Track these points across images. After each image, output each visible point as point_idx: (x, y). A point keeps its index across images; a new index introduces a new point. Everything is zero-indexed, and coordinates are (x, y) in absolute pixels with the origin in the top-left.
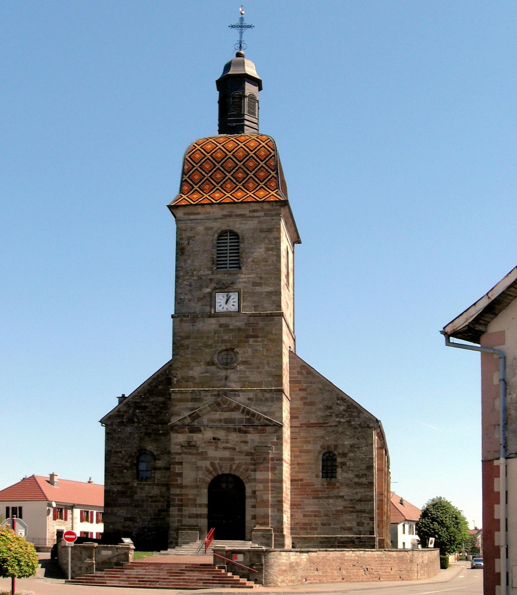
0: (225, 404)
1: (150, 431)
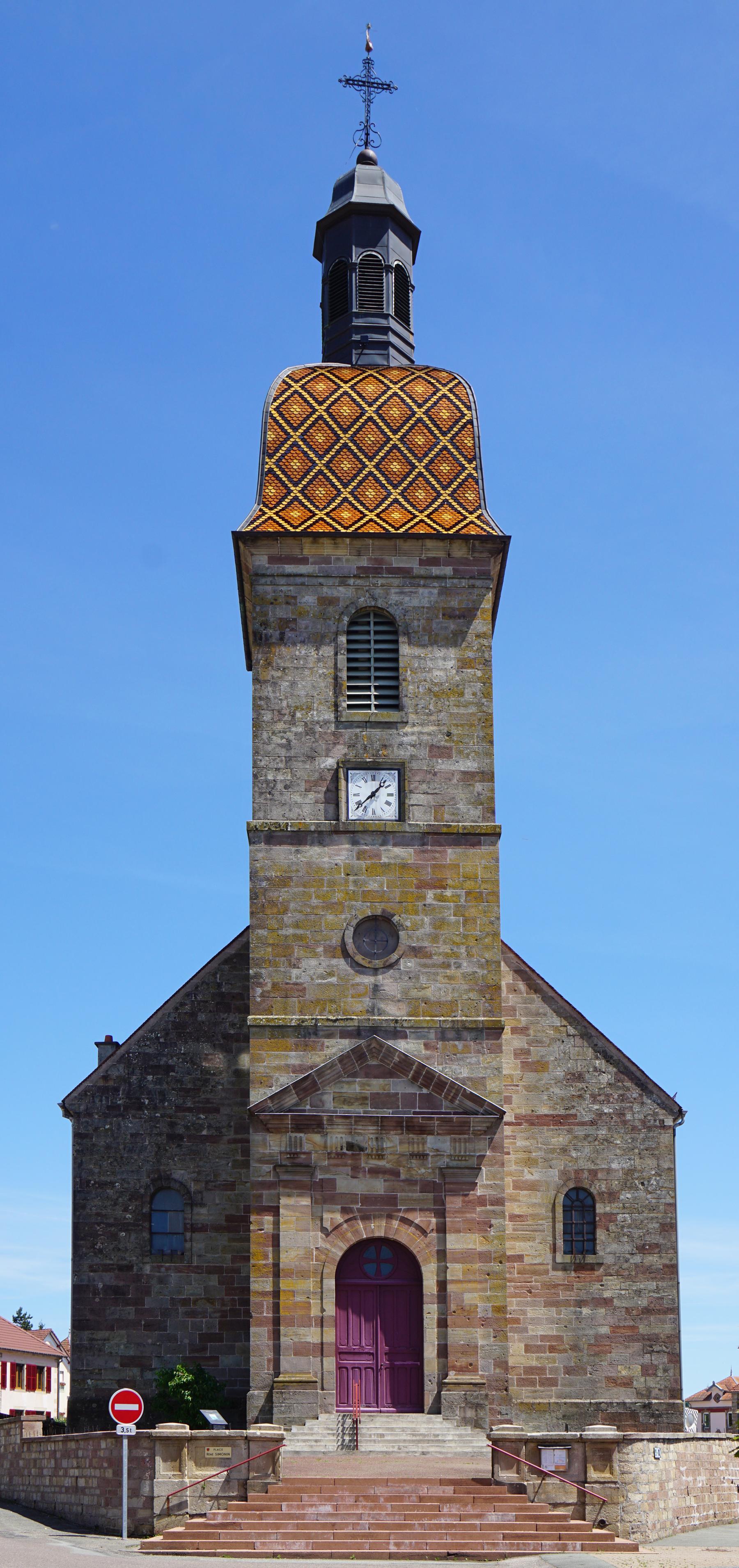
1: (180, 1130)
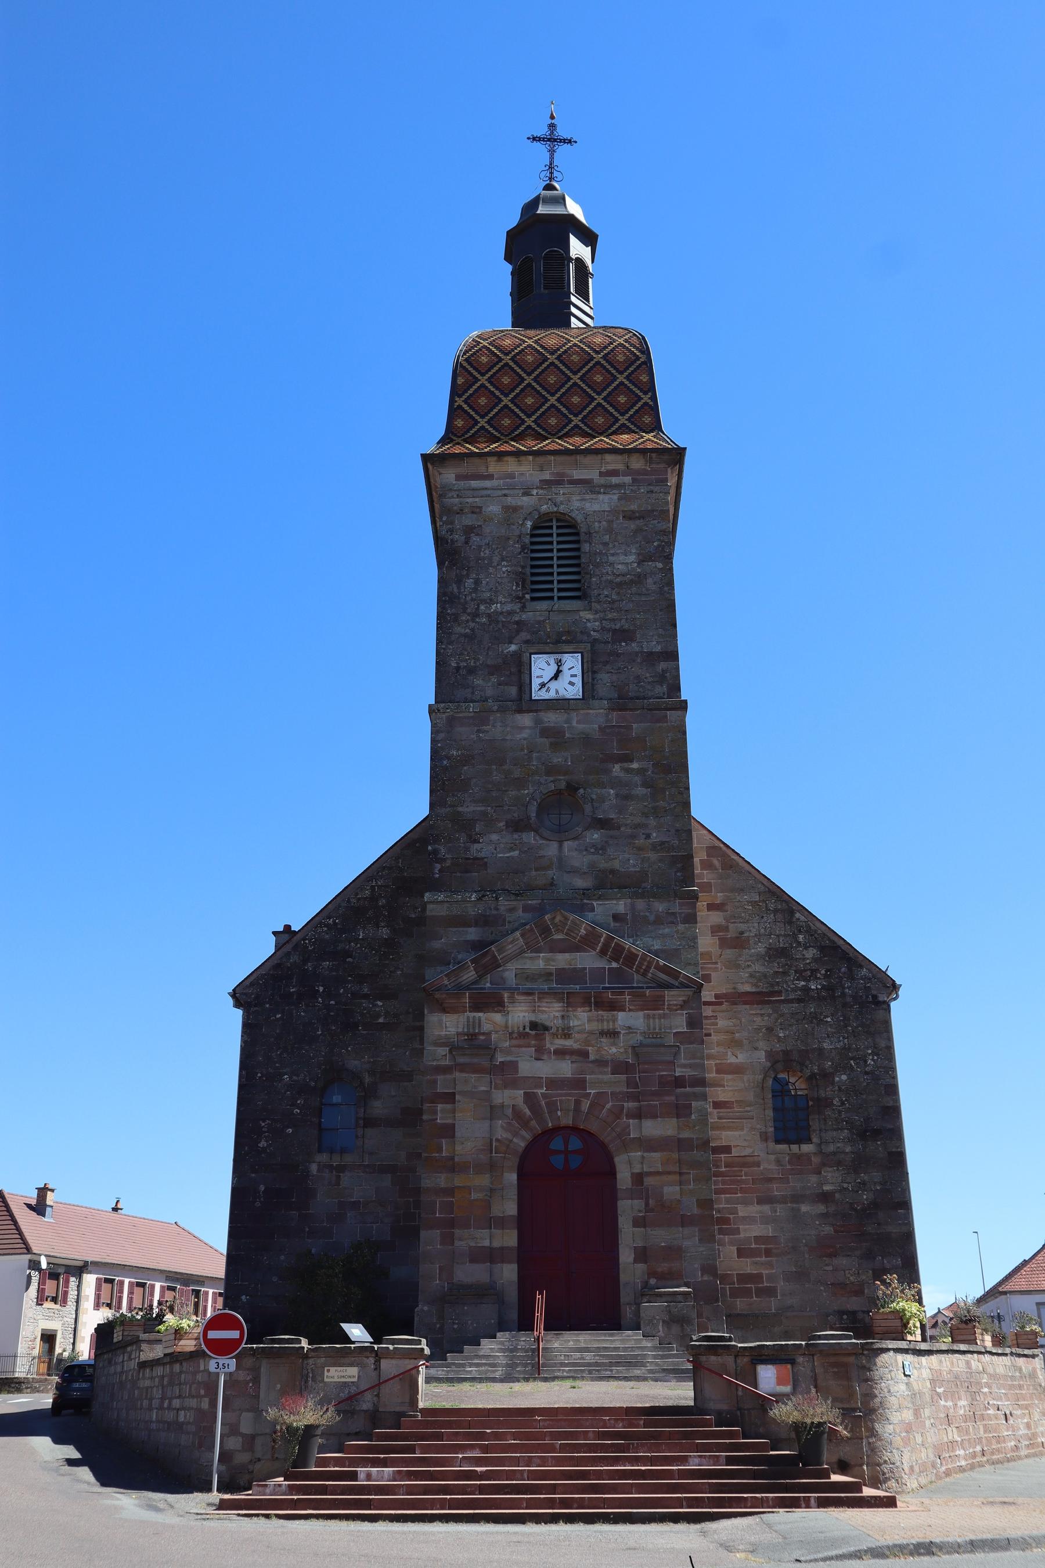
0: (558, 931)
